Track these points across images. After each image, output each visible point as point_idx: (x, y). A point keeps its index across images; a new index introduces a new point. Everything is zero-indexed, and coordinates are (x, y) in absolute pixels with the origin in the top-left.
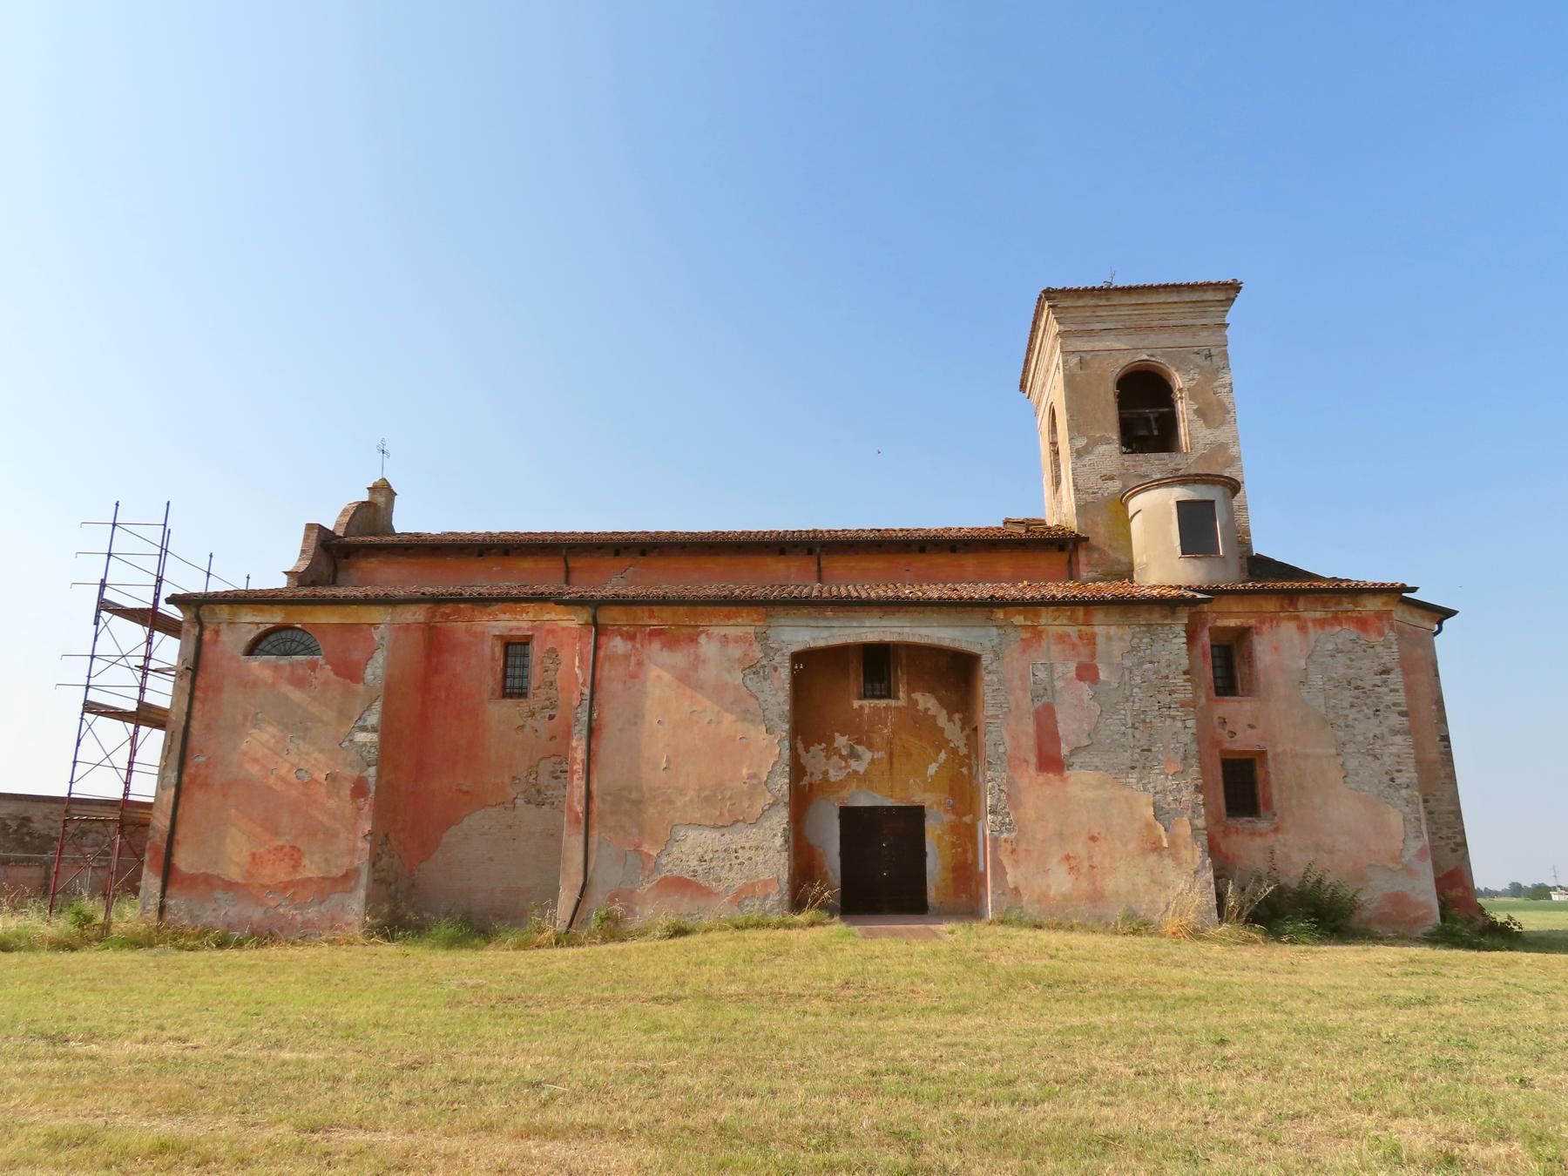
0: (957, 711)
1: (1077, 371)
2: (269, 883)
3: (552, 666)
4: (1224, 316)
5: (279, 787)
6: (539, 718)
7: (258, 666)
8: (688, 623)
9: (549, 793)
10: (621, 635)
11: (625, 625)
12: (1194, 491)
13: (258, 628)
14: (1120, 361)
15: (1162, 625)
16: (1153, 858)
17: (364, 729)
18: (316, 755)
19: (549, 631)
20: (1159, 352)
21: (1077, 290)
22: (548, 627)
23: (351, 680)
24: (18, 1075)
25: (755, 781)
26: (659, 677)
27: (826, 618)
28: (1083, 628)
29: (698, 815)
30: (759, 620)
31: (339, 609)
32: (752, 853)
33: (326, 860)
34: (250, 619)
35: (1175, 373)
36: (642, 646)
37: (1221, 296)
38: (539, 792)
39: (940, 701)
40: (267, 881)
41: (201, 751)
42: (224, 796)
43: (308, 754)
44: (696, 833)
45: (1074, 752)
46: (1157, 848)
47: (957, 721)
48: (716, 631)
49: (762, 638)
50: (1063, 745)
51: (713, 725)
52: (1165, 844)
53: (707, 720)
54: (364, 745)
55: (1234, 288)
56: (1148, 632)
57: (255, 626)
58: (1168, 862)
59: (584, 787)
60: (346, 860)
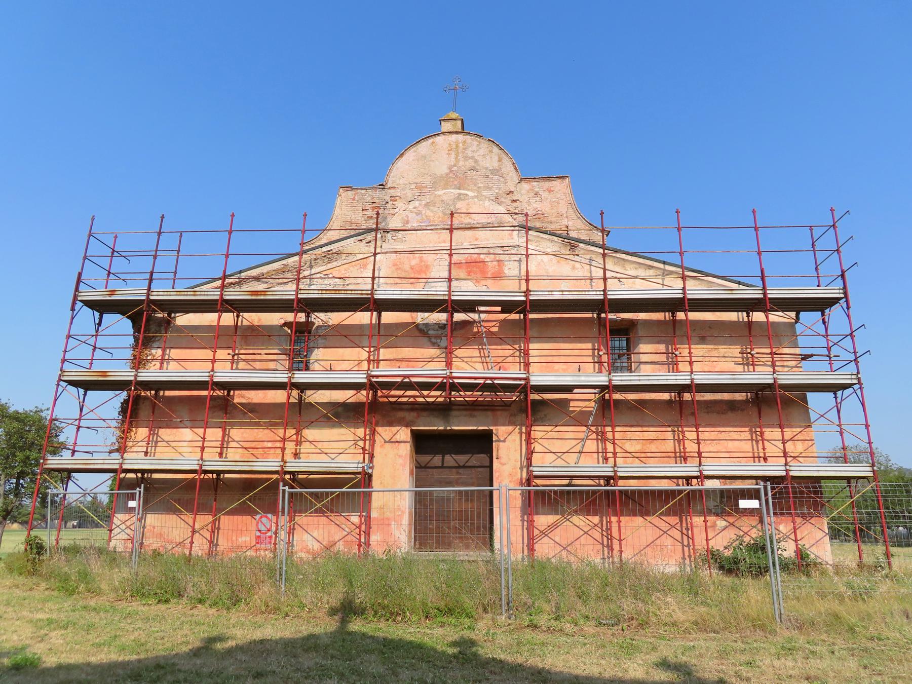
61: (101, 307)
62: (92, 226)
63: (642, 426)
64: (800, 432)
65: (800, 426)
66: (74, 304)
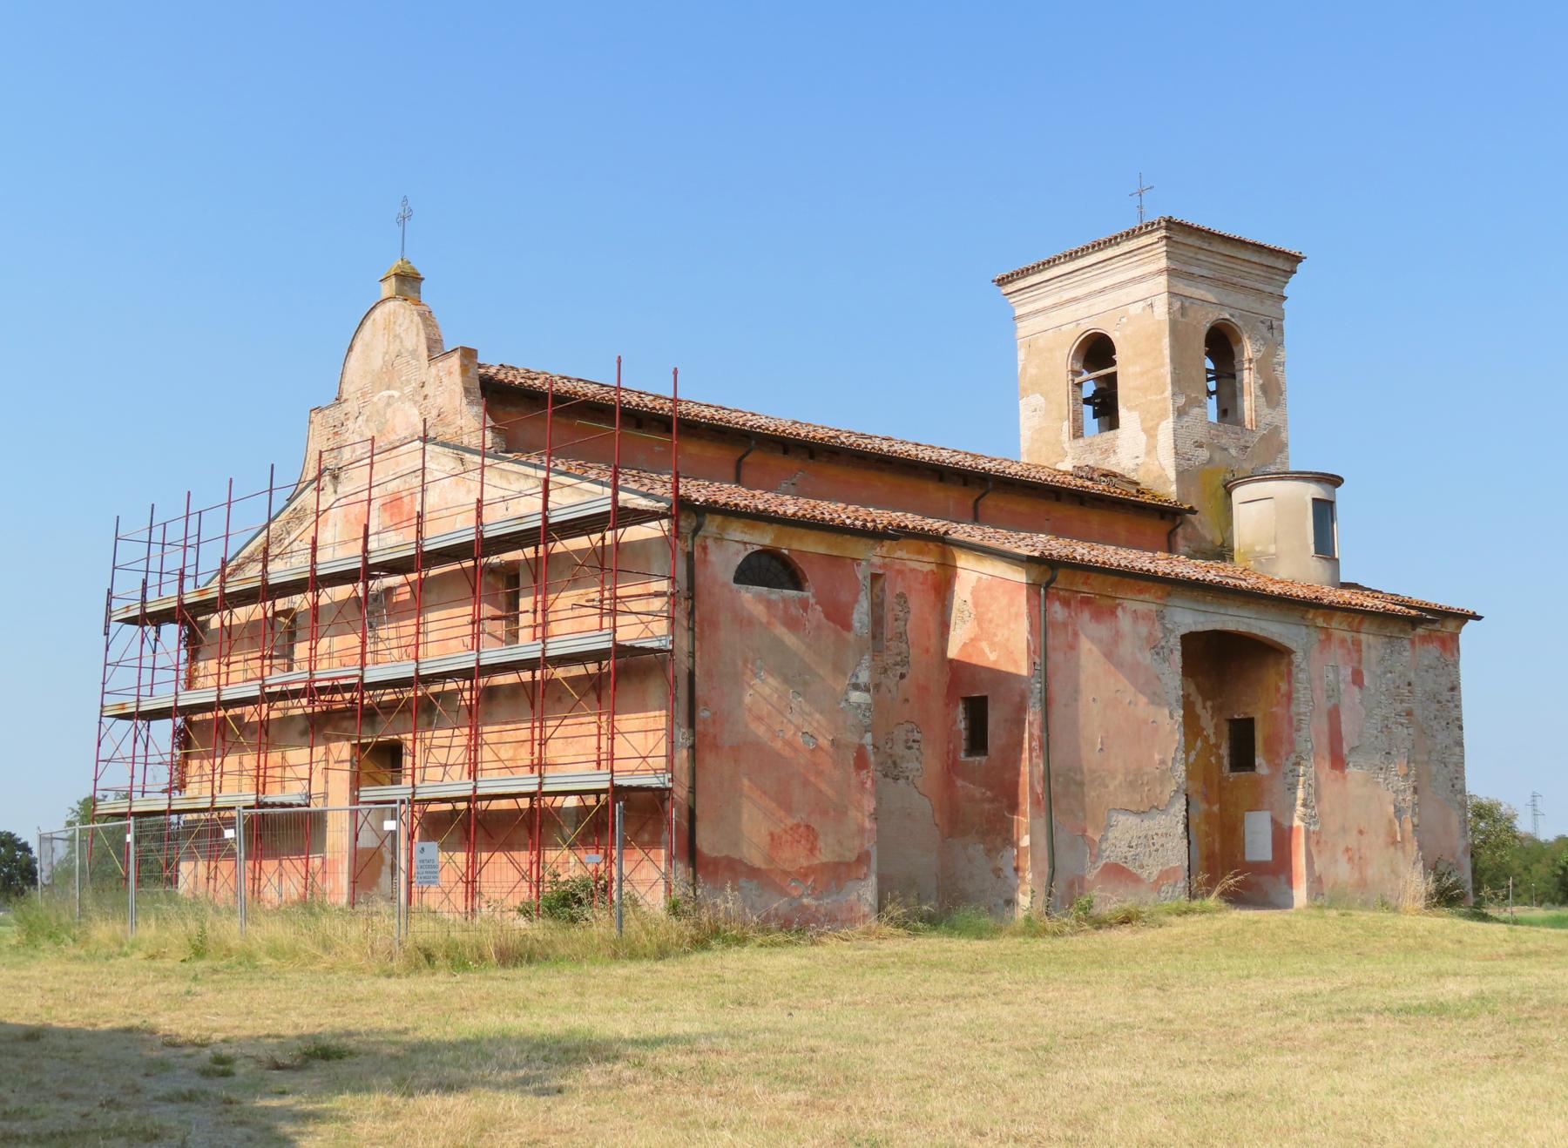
0: (1209, 699)
1: (1178, 316)
2: (789, 870)
3: (901, 614)
4: (1283, 288)
5: (787, 752)
6: (891, 675)
7: (751, 597)
8: (1109, 594)
9: (904, 765)
10: (1059, 599)
11: (1062, 589)
12: (1325, 490)
13: (746, 549)
14: (1210, 315)
15: (1397, 638)
16: (1392, 849)
17: (856, 687)
18: (817, 716)
19: (900, 572)
20: (1237, 313)
21: (1190, 227)
22: (897, 567)
23: (842, 627)
24: (1085, 1039)
25: (1164, 767)
26: (1090, 650)
27: (1205, 603)
28: (1355, 634)
29: (1125, 800)
30: (1161, 598)
31: (832, 538)
32: (1163, 840)
33: (840, 843)
34: (739, 536)
35: (1247, 341)
36: (1076, 614)
37: (1280, 264)
38: (894, 763)
39: (1198, 687)
40: (787, 867)
41: (706, 704)
42: (735, 761)
43: (810, 715)
44: (1124, 818)
45: (1353, 749)
46: (1394, 843)
47: (1209, 709)
48: (1130, 605)
49: (1161, 616)
50: (1344, 745)
51: (1132, 706)
52: (1399, 839)
53: (1128, 700)
54: (859, 706)
55: (1296, 259)
56: (1390, 643)
57: (741, 547)
58: (1400, 853)
59: (1042, 766)
60: (857, 842)
61: (151, 619)
62: (152, 518)
63: (514, 722)
64: (558, 727)
65: (557, 719)
66: (107, 626)
